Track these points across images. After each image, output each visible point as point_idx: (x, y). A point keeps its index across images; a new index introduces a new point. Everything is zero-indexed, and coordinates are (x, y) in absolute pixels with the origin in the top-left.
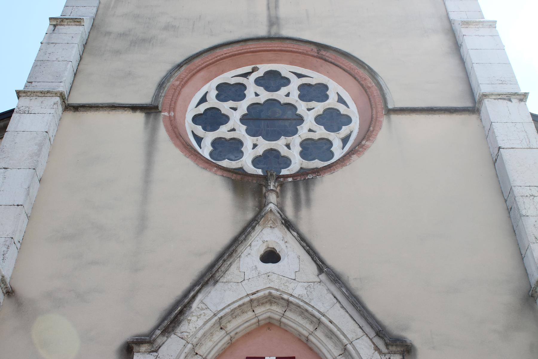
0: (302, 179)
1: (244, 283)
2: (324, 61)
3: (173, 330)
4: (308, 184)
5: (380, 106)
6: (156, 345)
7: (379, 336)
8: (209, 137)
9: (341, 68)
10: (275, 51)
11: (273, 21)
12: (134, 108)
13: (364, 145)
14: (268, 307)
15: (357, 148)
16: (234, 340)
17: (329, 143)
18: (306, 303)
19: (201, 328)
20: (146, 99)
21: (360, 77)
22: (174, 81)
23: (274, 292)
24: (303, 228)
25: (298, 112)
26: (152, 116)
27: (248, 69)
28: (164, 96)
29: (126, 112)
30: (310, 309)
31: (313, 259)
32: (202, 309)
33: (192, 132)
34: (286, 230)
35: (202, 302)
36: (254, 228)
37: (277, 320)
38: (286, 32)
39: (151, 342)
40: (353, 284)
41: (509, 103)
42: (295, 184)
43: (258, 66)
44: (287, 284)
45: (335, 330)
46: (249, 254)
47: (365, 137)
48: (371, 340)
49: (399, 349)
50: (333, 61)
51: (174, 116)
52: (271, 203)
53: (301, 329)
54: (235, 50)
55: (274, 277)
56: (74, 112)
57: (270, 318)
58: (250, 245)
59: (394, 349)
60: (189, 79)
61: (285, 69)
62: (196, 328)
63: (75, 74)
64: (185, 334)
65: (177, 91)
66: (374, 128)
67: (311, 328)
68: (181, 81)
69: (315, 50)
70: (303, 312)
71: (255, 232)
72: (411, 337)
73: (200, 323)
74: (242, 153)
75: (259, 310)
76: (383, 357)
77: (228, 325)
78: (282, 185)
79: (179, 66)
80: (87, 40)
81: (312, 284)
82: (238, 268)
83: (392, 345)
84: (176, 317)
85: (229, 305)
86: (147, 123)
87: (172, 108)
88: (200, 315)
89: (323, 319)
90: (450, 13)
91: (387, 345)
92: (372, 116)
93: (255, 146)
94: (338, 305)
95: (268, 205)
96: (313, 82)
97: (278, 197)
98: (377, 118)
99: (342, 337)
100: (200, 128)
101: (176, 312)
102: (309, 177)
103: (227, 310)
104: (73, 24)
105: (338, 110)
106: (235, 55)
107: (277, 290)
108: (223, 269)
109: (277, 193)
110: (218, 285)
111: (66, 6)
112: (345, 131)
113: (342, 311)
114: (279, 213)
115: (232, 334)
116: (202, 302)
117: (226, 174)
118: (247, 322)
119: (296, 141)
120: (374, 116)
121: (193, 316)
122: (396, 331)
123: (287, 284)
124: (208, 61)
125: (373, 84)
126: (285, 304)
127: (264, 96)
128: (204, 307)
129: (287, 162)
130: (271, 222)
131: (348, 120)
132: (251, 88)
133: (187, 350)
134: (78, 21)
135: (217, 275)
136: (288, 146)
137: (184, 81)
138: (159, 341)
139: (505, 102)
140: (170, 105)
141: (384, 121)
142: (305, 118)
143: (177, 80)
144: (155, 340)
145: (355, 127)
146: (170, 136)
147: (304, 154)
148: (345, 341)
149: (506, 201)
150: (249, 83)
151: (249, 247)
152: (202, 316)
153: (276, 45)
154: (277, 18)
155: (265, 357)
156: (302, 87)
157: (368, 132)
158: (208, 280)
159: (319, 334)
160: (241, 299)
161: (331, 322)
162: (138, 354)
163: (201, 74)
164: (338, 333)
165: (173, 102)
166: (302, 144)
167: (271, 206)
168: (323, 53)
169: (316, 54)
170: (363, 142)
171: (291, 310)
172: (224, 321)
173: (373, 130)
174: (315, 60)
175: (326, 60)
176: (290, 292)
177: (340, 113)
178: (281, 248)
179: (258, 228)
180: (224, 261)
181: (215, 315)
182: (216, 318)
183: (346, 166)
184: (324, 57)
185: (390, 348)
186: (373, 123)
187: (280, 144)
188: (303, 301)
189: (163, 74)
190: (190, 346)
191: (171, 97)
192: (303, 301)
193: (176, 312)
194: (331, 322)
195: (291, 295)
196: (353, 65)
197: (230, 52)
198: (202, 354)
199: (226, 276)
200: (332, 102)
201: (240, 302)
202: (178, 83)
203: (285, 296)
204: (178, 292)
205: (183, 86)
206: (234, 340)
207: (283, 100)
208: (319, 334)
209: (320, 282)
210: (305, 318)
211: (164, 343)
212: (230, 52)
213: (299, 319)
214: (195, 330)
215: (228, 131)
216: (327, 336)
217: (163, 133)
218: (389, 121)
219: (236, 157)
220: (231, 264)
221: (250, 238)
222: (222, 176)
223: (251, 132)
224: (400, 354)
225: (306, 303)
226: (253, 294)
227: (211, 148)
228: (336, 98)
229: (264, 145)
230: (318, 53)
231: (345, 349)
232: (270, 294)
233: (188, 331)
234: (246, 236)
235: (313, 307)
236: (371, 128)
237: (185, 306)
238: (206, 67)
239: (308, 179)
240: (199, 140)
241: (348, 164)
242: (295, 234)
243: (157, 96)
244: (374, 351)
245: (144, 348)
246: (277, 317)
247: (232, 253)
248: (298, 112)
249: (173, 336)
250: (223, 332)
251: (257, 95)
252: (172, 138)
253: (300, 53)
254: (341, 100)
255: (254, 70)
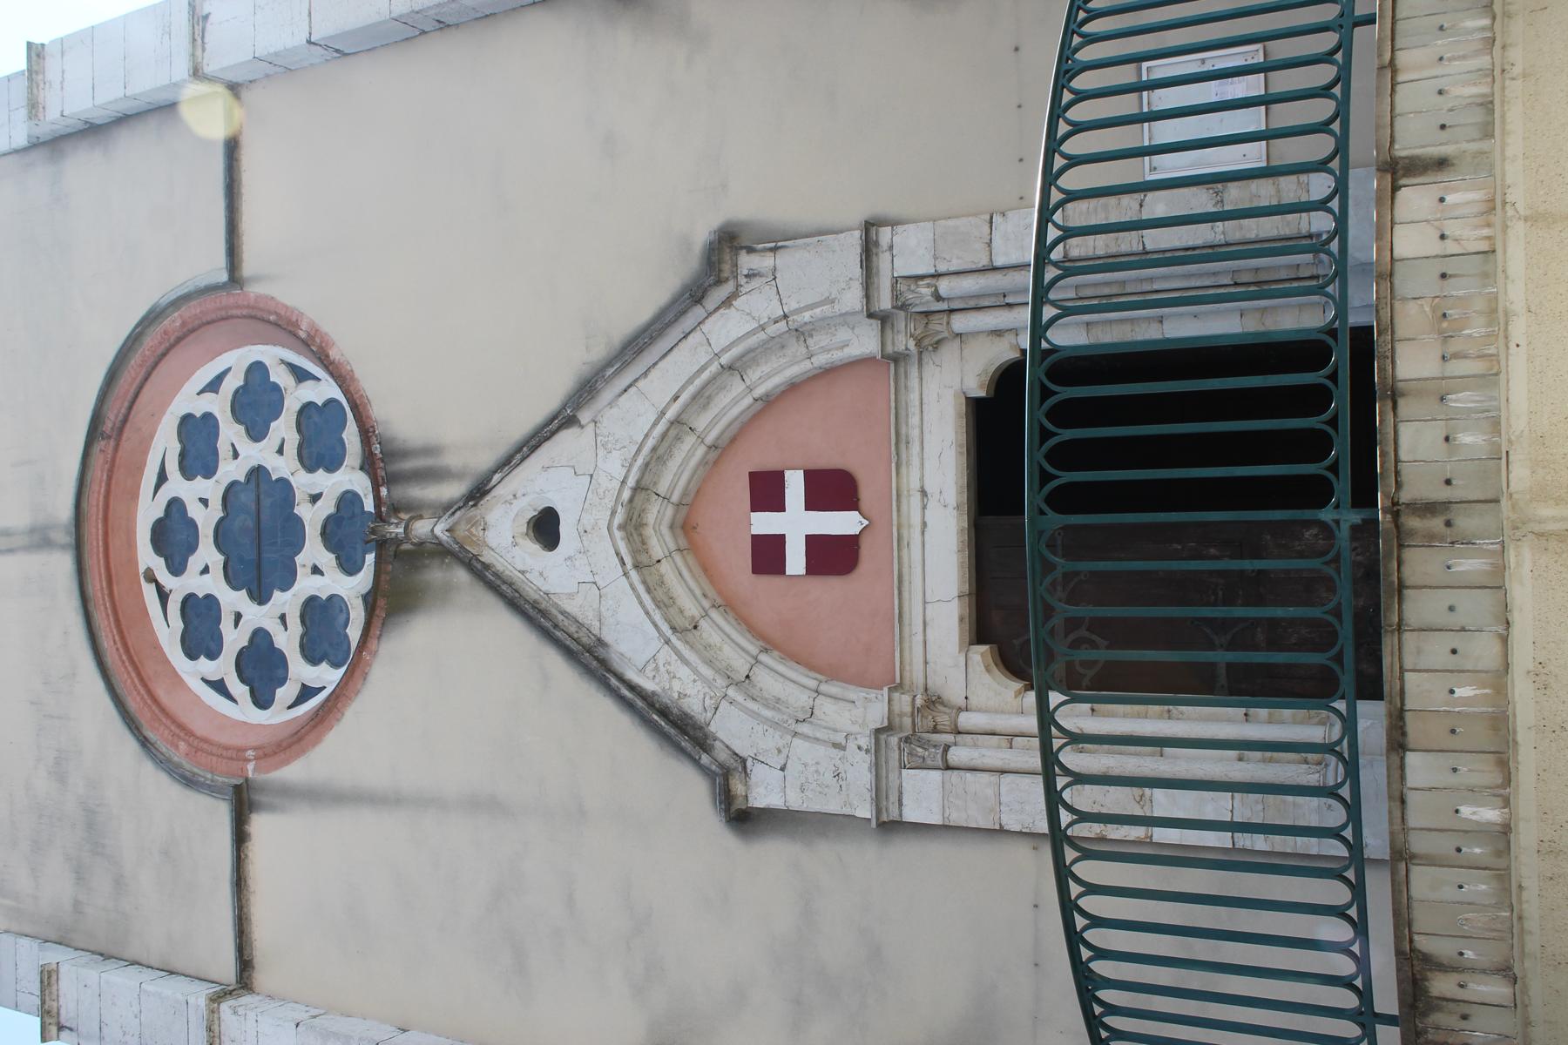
0: (382, 465)
1: (601, 584)
2: (128, 425)
3: (701, 728)
4: (394, 453)
5: (224, 299)
6: (731, 763)
7: (703, 297)
8: (301, 671)
9: (141, 387)
10: (106, 534)
11: (40, 539)
12: (240, 837)
13: (309, 335)
14: (649, 532)
15: (314, 348)
16: (719, 601)
17: (307, 409)
18: (639, 451)
19: (695, 671)
20: (222, 812)
21: (160, 343)
22: (179, 754)
23: (619, 518)
24: (484, 460)
25: (242, 479)
26: (256, 797)
27: (149, 592)
28: (212, 773)
29: (250, 855)
30: (650, 443)
31: (547, 439)
32: (657, 669)
33: (289, 708)
34: (488, 497)
35: (642, 671)
36: (487, 566)
37: (676, 512)
38: (63, 509)
39: (726, 773)
40: (599, 353)
41: (211, 19)
42: (393, 479)
43: (142, 570)
44: (601, 491)
45: (691, 389)
46: (541, 574)
47: (290, 332)
48: (710, 314)
49: (727, 257)
50: (126, 404)
51: (255, 749)
52: (432, 531)
53: (693, 462)
54: (106, 623)
55: (588, 520)
56: (253, 968)
57: (672, 527)
58: (523, 572)
59: (726, 268)
60: (174, 721)
61: (148, 510)
62: (695, 681)
63: (171, 973)
64: (708, 702)
65: (199, 744)
66: (270, 313)
67: (690, 440)
68: (179, 737)
69: (103, 443)
70: (657, 457)
71: (495, 563)
72: (702, 234)
73: (684, 672)
74: (331, 597)
75: (657, 550)
76: (743, 290)
77: (688, 613)
78: (396, 509)
79: (145, 743)
80: (93, 953)
81: (599, 439)
82: (571, 596)
83: (720, 271)
84: (674, 724)
85: (647, 613)
86: (271, 808)
87: (238, 754)
88: (669, 673)
89: (670, 414)
90: (15, 146)
91: (719, 282)
92: (244, 317)
93: (316, 570)
94: (641, 384)
95: (437, 538)
96: (175, 448)
97: (421, 517)
98: (248, 307)
99: (705, 376)
100: (280, 692)
101: (663, 724)
102: (378, 452)
103: (657, 616)
104: (55, 988)
105: (237, 392)
106: (117, 621)
107: (613, 513)
108: (572, 629)
109: (412, 519)
110: (608, 637)
111: (16, 1007)
112: (280, 377)
113: (654, 374)
114: (453, 513)
115: (706, 604)
116: (642, 671)
117: (375, 631)
118: (680, 574)
119: (303, 482)
120: (245, 312)
121: (671, 688)
122: (685, 268)
123: (601, 491)
124: (133, 682)
125: (176, 314)
126: (641, 496)
127: (207, 553)
128: (651, 666)
129: (348, 500)
130: (473, 530)
131: (257, 370)
132: (193, 582)
133: (740, 698)
134: (48, 978)
135: (585, 640)
136: (315, 498)
137: (177, 731)
138: (723, 756)
139: (209, 27)
140: (231, 759)
141: (254, 290)
142: (255, 463)
143: (177, 747)
144: (721, 766)
145: (272, 355)
146: (298, 755)
147: (331, 462)
148: (714, 368)
149: (423, 32)
150: (179, 587)
151: (527, 575)
152: (672, 669)
153: (94, 530)
154: (32, 531)
155: (754, 537)
156: (187, 472)
157: (279, 326)
158: (596, 658)
159: (701, 423)
160: (633, 589)
161: (676, 398)
162: (750, 799)
163: (161, 693)
164: (698, 382)
165: (224, 753)
166: (310, 469)
167: (440, 530)
168: (108, 426)
169: (112, 443)
170: (302, 335)
171: (655, 483)
172: (681, 622)
173: (276, 313)
174: (126, 444)
175: (125, 421)
176: (617, 485)
177: (241, 387)
178: (528, 508)
179: (487, 557)
180: (556, 626)
181: (668, 642)
182: (674, 639)
183: (352, 371)
184: (118, 424)
185: (725, 275)
186: (259, 314)
187: (312, 517)
188: (635, 458)
189: (163, 778)
190: (731, 692)
191: (214, 758)
192: (635, 458)
193: (663, 724)
194: (676, 398)
195: (624, 482)
196: (135, 360)
197: (112, 632)
198: (748, 666)
199: (587, 622)
200: (218, 406)
201: (641, 589)
202: (182, 745)
203: (626, 495)
204: (623, 722)
205: (190, 733)
206: (719, 601)
207: (215, 511)
208: (701, 423)
209: (596, 423)
210: (670, 453)
211: (727, 747)
212: (112, 632)
213: (673, 465)
214: (699, 683)
215: (286, 629)
216: (705, 406)
217: (294, 772)
218: (257, 279)
219: (341, 611)
220: (563, 613)
221: (507, 572)
222: (379, 638)
223: (288, 579)
224: (737, 255)
225: (639, 451)
226: (623, 563)
227: (324, 665)
228: (209, 396)
229: (314, 551)
230: (109, 437)
231: (730, 368)
232: (622, 527)
233: (701, 696)
234: (504, 582)
235: (647, 436)
236: (272, 318)
237: (651, 705)
238: (145, 685)
239: (381, 452)
240: (306, 693)
241: (349, 368)
242: (497, 477)
243: (211, 789)
244: (733, 309)
245: (738, 787)
246: (670, 511)
247: (540, 611)
248: (242, 479)
249: (712, 728)
250: (703, 624)
251: (206, 570)
252: (303, 752)
253: (110, 478)
254: (214, 386)
255: (151, 577)
